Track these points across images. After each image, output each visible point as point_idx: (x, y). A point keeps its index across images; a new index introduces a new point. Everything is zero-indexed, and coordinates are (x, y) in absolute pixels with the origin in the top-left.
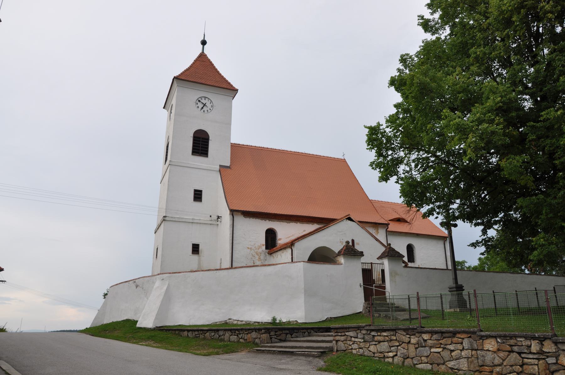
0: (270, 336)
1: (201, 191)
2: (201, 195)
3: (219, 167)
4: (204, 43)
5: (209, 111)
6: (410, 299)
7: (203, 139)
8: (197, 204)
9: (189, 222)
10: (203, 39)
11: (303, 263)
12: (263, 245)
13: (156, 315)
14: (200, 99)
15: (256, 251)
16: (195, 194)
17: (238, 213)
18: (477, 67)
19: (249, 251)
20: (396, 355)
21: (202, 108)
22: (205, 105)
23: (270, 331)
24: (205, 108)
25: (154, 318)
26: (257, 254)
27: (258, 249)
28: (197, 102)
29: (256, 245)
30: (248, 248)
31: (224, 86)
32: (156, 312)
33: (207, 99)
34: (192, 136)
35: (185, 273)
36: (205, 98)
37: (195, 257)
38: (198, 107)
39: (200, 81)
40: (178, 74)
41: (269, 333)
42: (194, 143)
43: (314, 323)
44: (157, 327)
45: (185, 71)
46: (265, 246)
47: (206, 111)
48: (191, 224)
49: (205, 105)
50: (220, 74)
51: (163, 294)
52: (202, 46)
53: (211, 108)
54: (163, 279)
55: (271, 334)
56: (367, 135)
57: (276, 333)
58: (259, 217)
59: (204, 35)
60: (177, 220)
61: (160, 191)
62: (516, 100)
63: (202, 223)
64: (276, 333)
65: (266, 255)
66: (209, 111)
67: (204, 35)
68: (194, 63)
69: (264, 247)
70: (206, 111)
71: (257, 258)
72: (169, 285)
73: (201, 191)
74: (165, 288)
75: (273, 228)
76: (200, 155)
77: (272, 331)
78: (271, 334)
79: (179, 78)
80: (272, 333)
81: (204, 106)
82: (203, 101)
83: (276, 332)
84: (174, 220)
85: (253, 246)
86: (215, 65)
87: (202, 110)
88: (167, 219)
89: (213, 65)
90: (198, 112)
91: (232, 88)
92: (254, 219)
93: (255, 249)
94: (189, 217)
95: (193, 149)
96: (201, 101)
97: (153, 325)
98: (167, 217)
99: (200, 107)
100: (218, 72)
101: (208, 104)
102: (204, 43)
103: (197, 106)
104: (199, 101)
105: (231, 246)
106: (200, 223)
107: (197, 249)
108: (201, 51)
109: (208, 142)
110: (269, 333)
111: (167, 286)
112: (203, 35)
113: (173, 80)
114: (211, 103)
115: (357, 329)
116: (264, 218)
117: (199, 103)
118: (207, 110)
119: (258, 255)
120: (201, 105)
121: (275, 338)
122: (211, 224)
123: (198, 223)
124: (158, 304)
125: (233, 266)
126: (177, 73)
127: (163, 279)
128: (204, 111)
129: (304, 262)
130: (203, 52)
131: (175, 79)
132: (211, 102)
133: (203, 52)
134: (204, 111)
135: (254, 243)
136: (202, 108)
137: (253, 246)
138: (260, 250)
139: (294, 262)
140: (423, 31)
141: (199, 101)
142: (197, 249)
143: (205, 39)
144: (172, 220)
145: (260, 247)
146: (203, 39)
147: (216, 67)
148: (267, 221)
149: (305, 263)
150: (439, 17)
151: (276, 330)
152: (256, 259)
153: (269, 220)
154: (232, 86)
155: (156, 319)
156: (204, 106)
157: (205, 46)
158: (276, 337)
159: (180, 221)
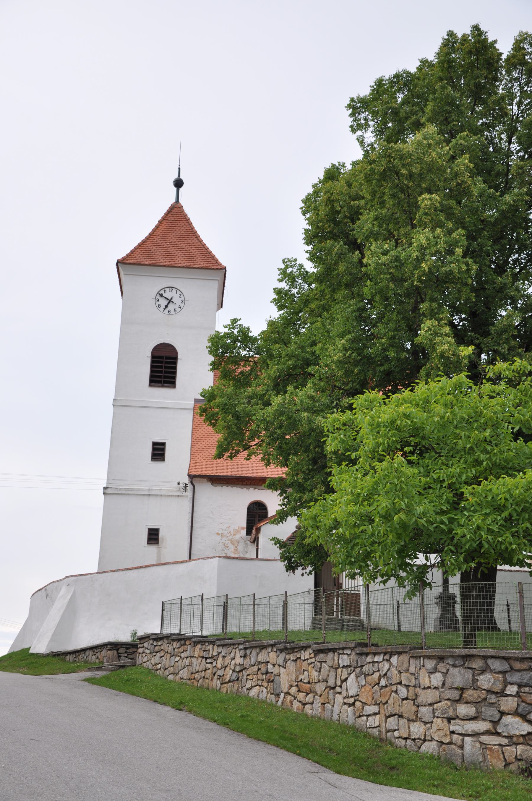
0: (118, 653)
1: (163, 444)
2: (163, 450)
3: (193, 402)
4: (179, 184)
5: (178, 310)
6: (510, 607)
7: (167, 358)
8: (158, 465)
9: (144, 495)
10: (177, 176)
11: (218, 558)
12: (243, 528)
13: (52, 635)
14: (162, 292)
15: (230, 538)
16: (154, 449)
17: (202, 479)
19: (219, 538)
20: (248, 675)
21: (166, 306)
22: (170, 301)
23: (118, 647)
24: (171, 307)
25: (48, 640)
26: (232, 543)
27: (235, 535)
28: (158, 297)
29: (231, 529)
30: (218, 534)
31: (203, 265)
32: (53, 631)
33: (174, 290)
34: (150, 355)
35: (92, 576)
36: (171, 288)
37: (153, 549)
38: (159, 306)
39: (162, 262)
40: (124, 254)
41: (118, 650)
42: (152, 366)
44: (53, 652)
45: (140, 245)
46: (245, 530)
47: (172, 312)
48: (146, 497)
49: (170, 301)
50: (201, 241)
51: (65, 606)
52: (175, 189)
53: (182, 305)
54: (69, 585)
55: (119, 652)
57: (128, 651)
58: (237, 484)
59: (179, 168)
60: (124, 492)
63: (165, 496)
64: (128, 651)
65: (247, 544)
66: (178, 310)
67: (179, 168)
68: (157, 227)
69: (244, 532)
70: (172, 312)
71: (233, 550)
72: (74, 592)
73: (163, 444)
74: (69, 597)
75: (261, 501)
76: (163, 386)
77: (121, 648)
78: (119, 652)
79: (124, 261)
80: (122, 650)
81: (168, 303)
82: (168, 295)
83: (127, 649)
84: (119, 492)
85: (226, 530)
86: (194, 225)
87: (167, 310)
88: (108, 491)
89: (190, 224)
90: (159, 315)
91: (216, 266)
92: (229, 487)
93: (228, 535)
94: (144, 487)
95: (151, 376)
96: (164, 295)
97: (46, 649)
98: (109, 489)
99: (163, 306)
100: (198, 237)
101: (177, 299)
102: (179, 184)
103: (157, 304)
104: (161, 295)
105: (190, 532)
106: (161, 495)
107: (155, 537)
108: (174, 200)
109: (176, 363)
110: (118, 650)
111: (71, 594)
112: (178, 170)
113: (117, 265)
114: (182, 296)
115: (291, 651)
116: (247, 485)
117: (160, 299)
118: (175, 310)
119: (234, 545)
120: (163, 302)
121: (126, 657)
122: (178, 496)
123: (157, 495)
124: (57, 620)
125: (259, 557)
126: (120, 257)
127: (69, 585)
128: (169, 312)
129: (219, 557)
130: (177, 201)
131: (119, 264)
132: (181, 294)
133: (177, 201)
134: (169, 312)
135: (228, 526)
136: (166, 306)
137: (226, 530)
138: (238, 537)
139: (193, 560)
141: (161, 295)
142: (155, 537)
143: (181, 177)
144: (116, 492)
145: (237, 532)
146: (176, 176)
147: (195, 228)
148: (252, 489)
149: (221, 559)
151: (128, 647)
152: (231, 550)
153: (255, 488)
154: (217, 261)
155: (52, 640)
156: (168, 303)
157: (181, 189)
158: (126, 655)
159: (128, 494)
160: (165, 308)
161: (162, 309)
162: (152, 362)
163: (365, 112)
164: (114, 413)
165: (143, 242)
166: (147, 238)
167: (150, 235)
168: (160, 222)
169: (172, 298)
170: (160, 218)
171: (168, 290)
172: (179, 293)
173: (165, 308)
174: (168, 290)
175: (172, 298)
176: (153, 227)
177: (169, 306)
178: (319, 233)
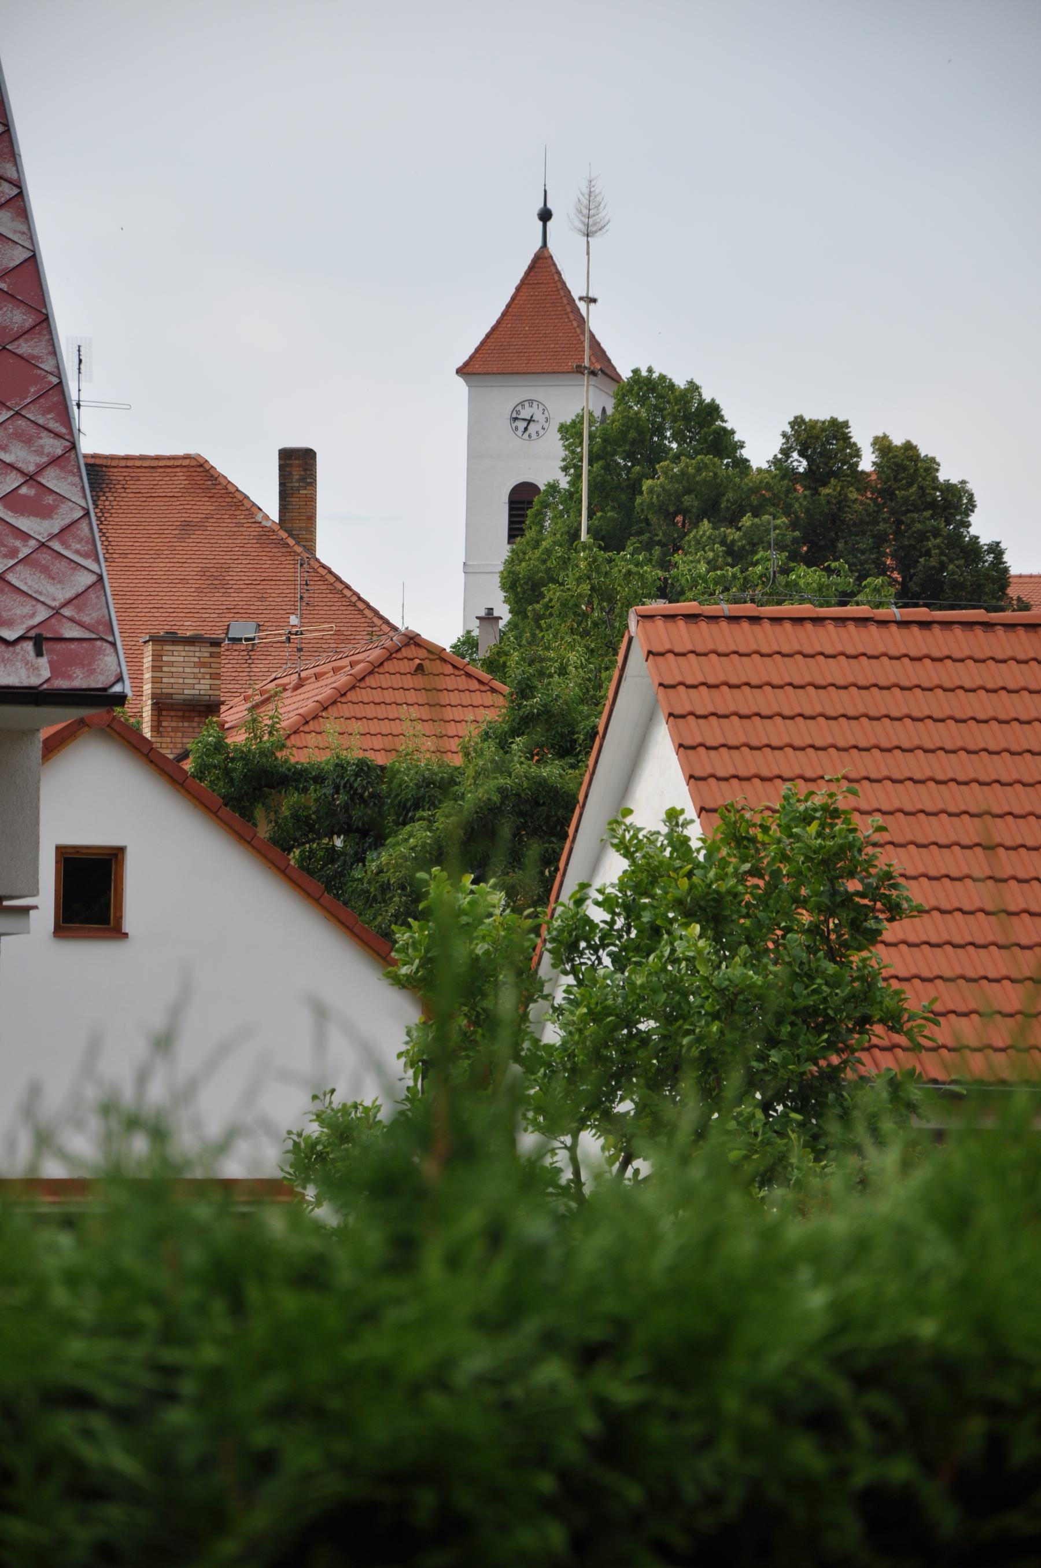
4: (545, 216)
14: (514, 415)
18: (875, 866)
21: (526, 429)
24: (533, 428)
33: (535, 404)
34: (507, 501)
36: (531, 402)
38: (517, 428)
42: (511, 516)
43: (21, 264)
45: (488, 336)
49: (530, 421)
52: (541, 224)
53: (546, 426)
56: (693, 387)
61: (376, 613)
62: (787, 468)
66: (541, 432)
70: (534, 436)
82: (525, 414)
102: (545, 216)
103: (514, 425)
114: (546, 412)
118: (537, 432)
120: (522, 425)
128: (530, 436)
134: (530, 436)
136: (526, 429)
140: (811, 414)
141: (516, 419)
143: (549, 206)
150: (855, 1156)
160: (524, 432)
161: (520, 433)
162: (511, 509)
163: (928, 494)
164: (465, 583)
165: (494, 329)
166: (499, 322)
167: (504, 314)
168: (518, 289)
169: (532, 417)
170: (517, 282)
171: (526, 404)
172: (541, 407)
173: (524, 432)
174: (526, 404)
175: (532, 417)
176: (507, 299)
177: (529, 427)
178: (847, 1027)
